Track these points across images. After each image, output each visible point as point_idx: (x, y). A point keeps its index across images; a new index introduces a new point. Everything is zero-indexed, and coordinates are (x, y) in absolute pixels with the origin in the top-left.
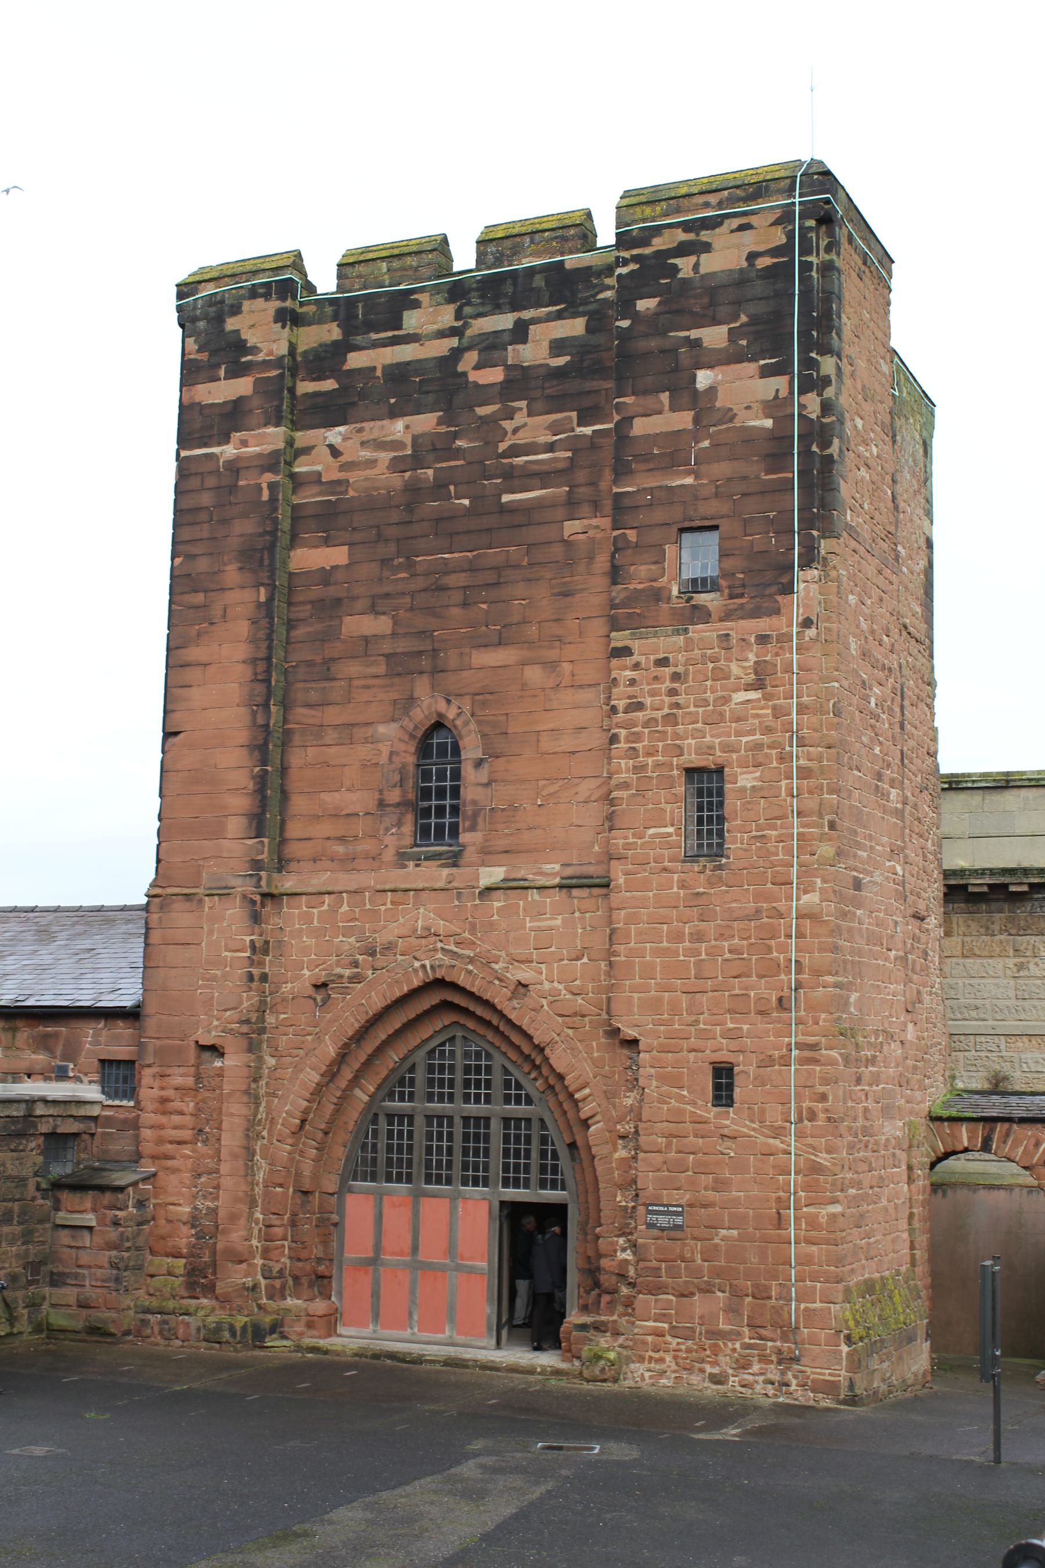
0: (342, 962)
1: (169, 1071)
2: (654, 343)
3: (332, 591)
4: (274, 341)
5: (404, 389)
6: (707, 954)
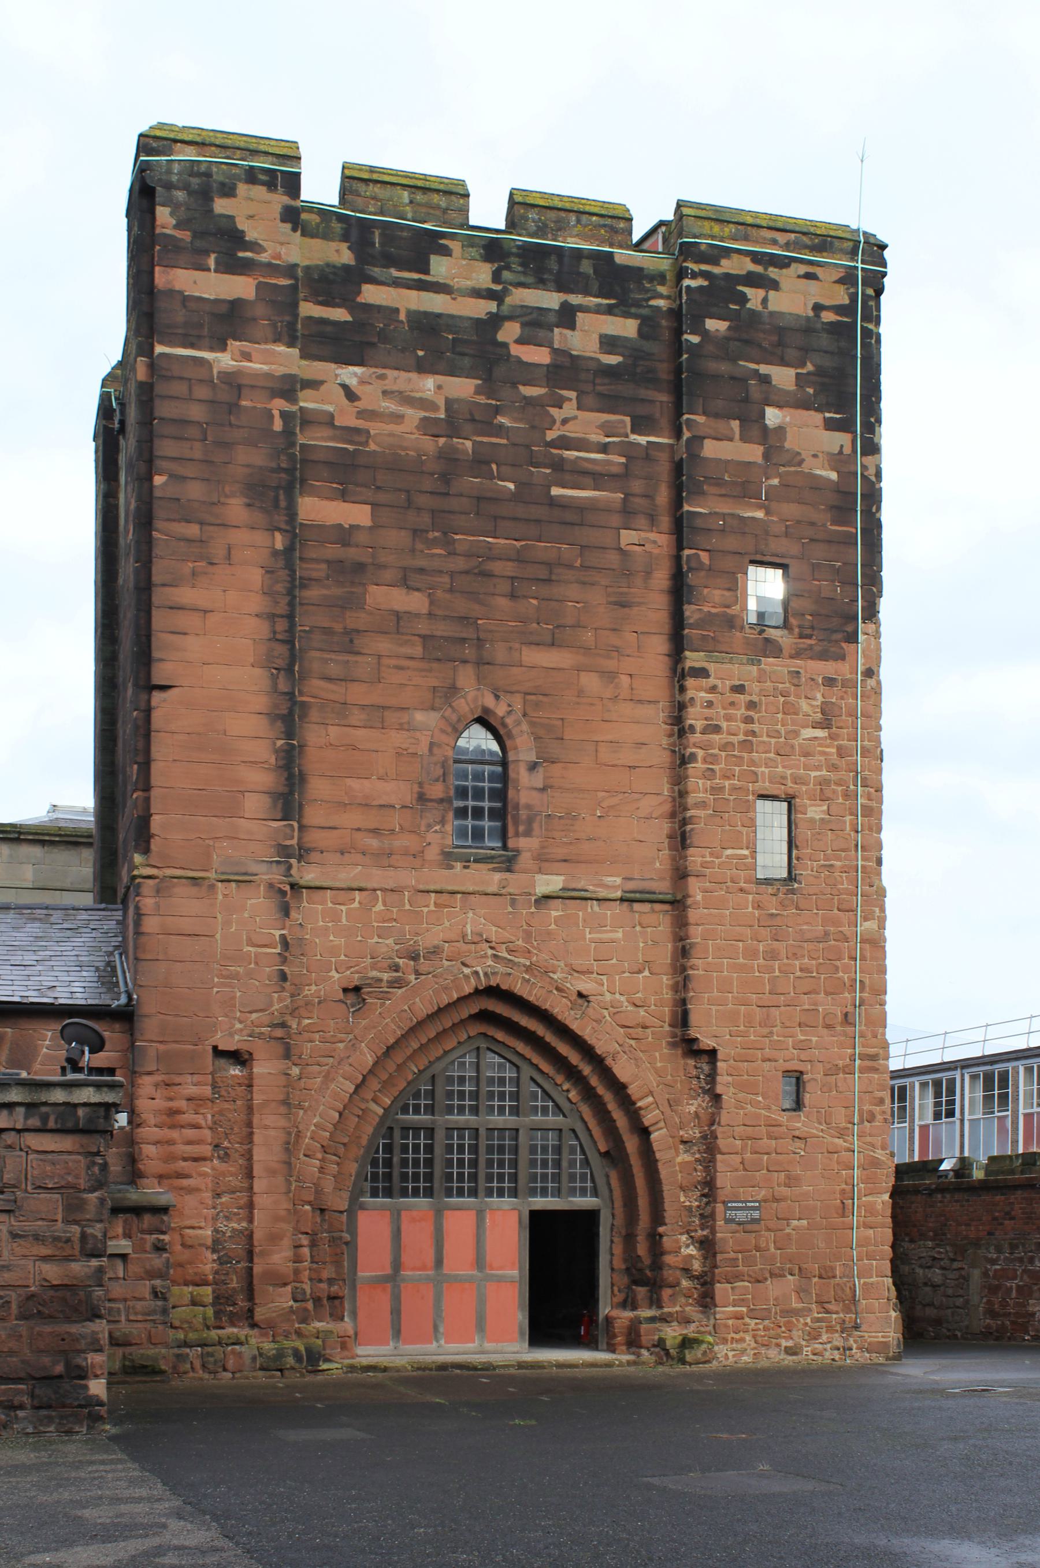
0: (379, 965)
1: (177, 1079)
2: (723, 368)
3: (352, 554)
4: (282, 244)
5: (433, 343)
6: (780, 971)
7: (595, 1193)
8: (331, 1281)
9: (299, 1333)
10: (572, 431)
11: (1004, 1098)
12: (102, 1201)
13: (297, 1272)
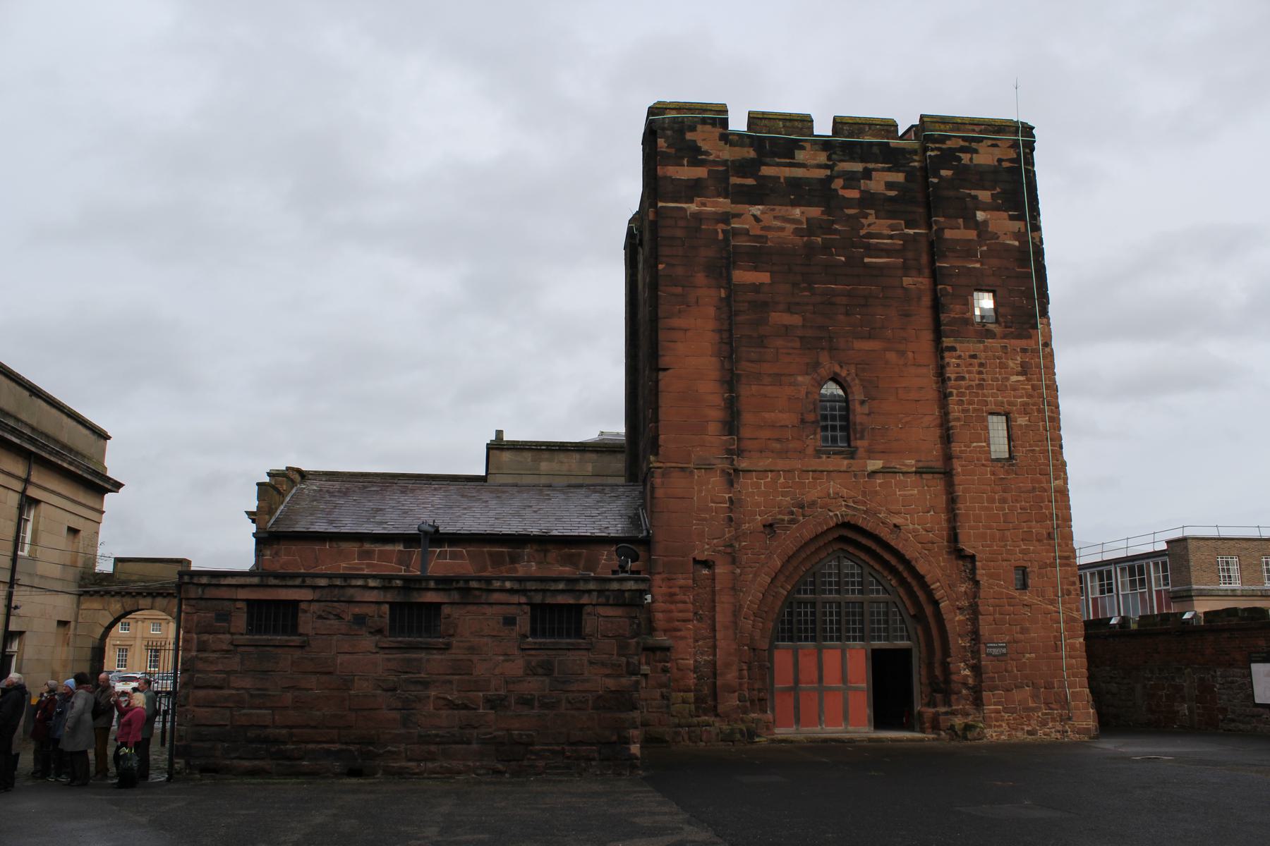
2: (951, 193)
5: (798, 191)
7: (909, 639)
8: (760, 690)
9: (743, 721)
10: (873, 230)
11: (1142, 581)
12: (638, 643)
13: (741, 684)
